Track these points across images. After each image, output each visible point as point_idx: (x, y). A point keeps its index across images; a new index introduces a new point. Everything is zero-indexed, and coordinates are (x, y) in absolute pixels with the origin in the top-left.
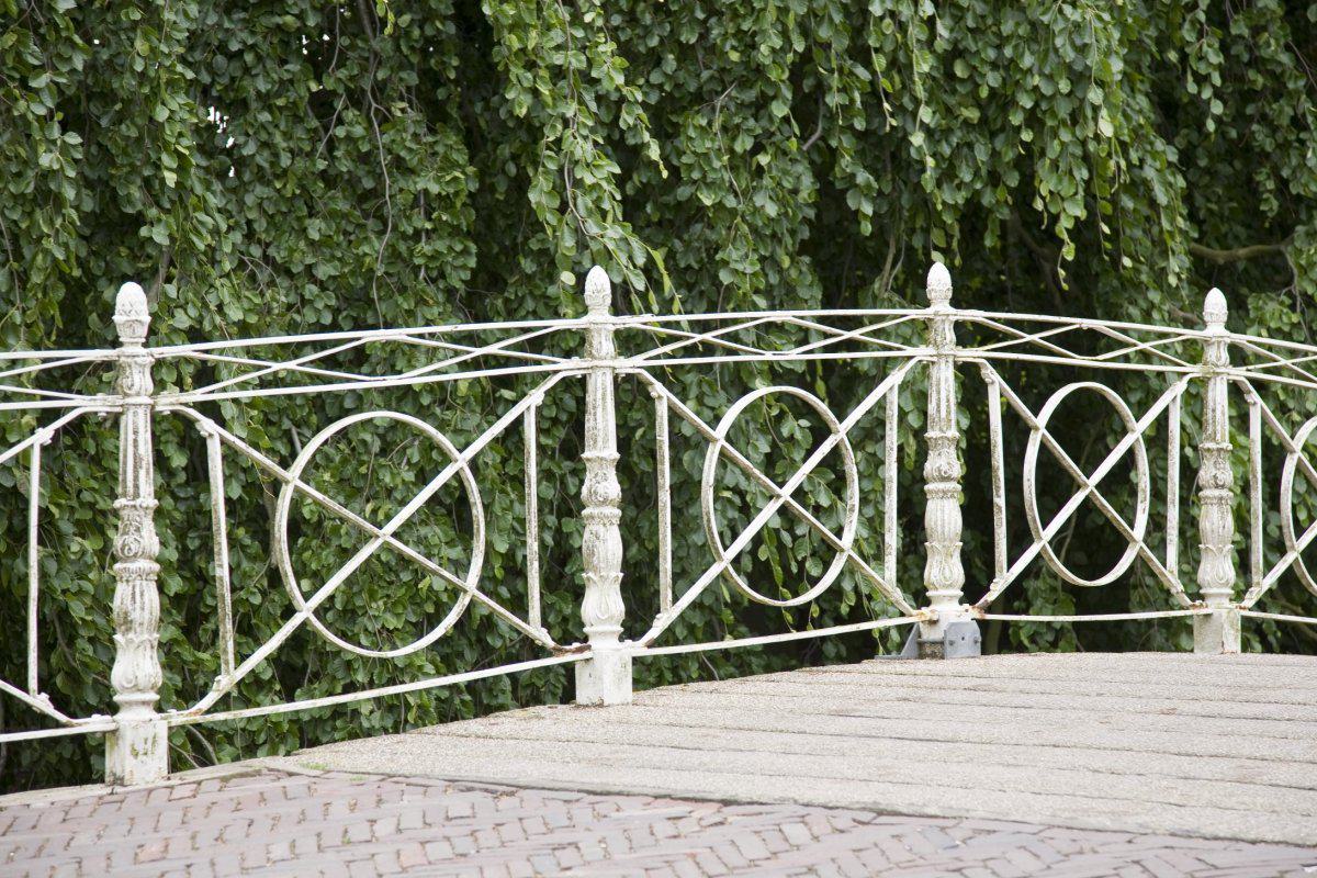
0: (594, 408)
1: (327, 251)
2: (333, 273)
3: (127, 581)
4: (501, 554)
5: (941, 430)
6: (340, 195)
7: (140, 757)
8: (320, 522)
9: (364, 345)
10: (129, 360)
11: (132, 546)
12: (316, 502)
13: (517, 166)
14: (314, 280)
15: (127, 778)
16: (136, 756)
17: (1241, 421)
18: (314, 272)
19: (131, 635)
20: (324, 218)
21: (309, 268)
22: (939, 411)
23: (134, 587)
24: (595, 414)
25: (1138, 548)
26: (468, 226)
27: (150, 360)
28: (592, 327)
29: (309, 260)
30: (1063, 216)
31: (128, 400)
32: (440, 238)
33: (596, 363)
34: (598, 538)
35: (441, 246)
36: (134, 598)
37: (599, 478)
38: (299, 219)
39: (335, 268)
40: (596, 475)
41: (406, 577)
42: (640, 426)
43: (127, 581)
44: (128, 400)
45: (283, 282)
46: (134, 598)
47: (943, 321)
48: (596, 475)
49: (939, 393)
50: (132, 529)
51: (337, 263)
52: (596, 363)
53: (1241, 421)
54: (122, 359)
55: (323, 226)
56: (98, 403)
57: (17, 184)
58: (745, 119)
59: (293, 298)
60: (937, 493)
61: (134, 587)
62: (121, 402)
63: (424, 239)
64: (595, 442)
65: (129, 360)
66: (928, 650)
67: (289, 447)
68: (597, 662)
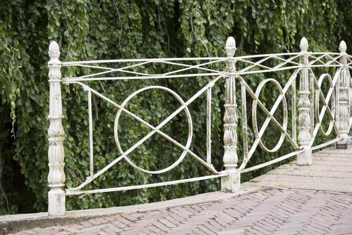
0: (304, 79)
1: (104, 33)
2: (106, 40)
3: (231, 130)
4: (159, 118)
5: (344, 87)
6: (104, 18)
7: (235, 184)
8: (112, 109)
9: (299, 57)
10: (232, 61)
11: (233, 119)
12: (110, 103)
13: (146, 13)
14: (101, 41)
15: (233, 190)
16: (234, 183)
17: (238, 88)
18: (101, 39)
19: (232, 146)
20: (102, 24)
21: (100, 38)
22: (343, 82)
23: (233, 132)
24: (304, 81)
25: (271, 117)
26: (140, 29)
27: (235, 61)
28: (304, 55)
29: (100, 36)
30: (292, 32)
31: (231, 73)
32: (135, 31)
33: (305, 66)
34: (306, 117)
35: (135, 33)
36: (233, 135)
37: (305, 99)
38: (96, 24)
39: (106, 38)
40: (305, 98)
41: (137, 124)
42: (181, 84)
43: (231, 130)
44: (231, 73)
45: (94, 42)
46: (233, 135)
47: (345, 57)
48: (305, 98)
49: (343, 77)
50: (232, 114)
51: (106, 37)
52: (305, 66)
53: (238, 88)
54: (230, 61)
55: (103, 26)
56: (224, 74)
57: (70, 7)
58: (223, 2)
59: (96, 46)
60: (343, 104)
61: (233, 132)
62: (229, 74)
63: (129, 32)
64: (305, 89)
65: (232, 61)
66: (339, 147)
67: (100, 87)
68: (306, 153)
